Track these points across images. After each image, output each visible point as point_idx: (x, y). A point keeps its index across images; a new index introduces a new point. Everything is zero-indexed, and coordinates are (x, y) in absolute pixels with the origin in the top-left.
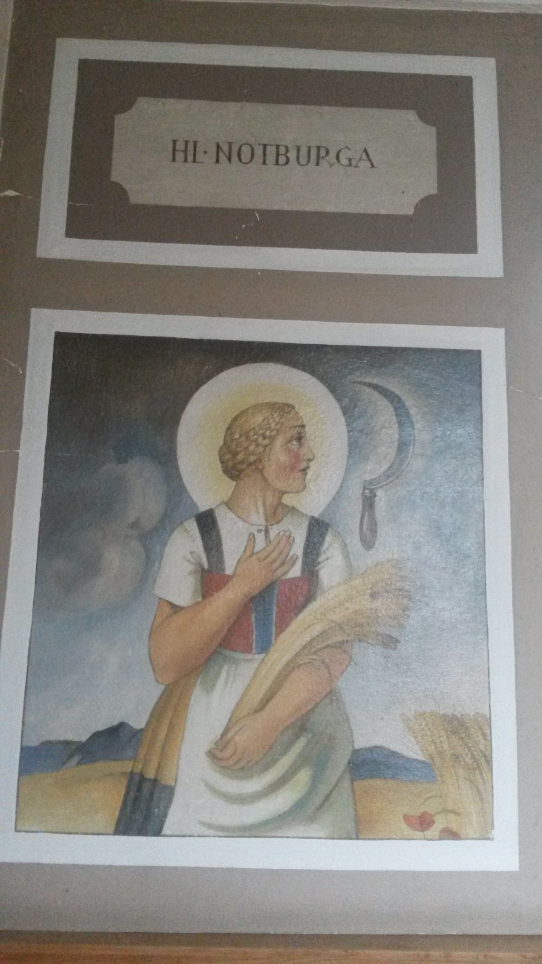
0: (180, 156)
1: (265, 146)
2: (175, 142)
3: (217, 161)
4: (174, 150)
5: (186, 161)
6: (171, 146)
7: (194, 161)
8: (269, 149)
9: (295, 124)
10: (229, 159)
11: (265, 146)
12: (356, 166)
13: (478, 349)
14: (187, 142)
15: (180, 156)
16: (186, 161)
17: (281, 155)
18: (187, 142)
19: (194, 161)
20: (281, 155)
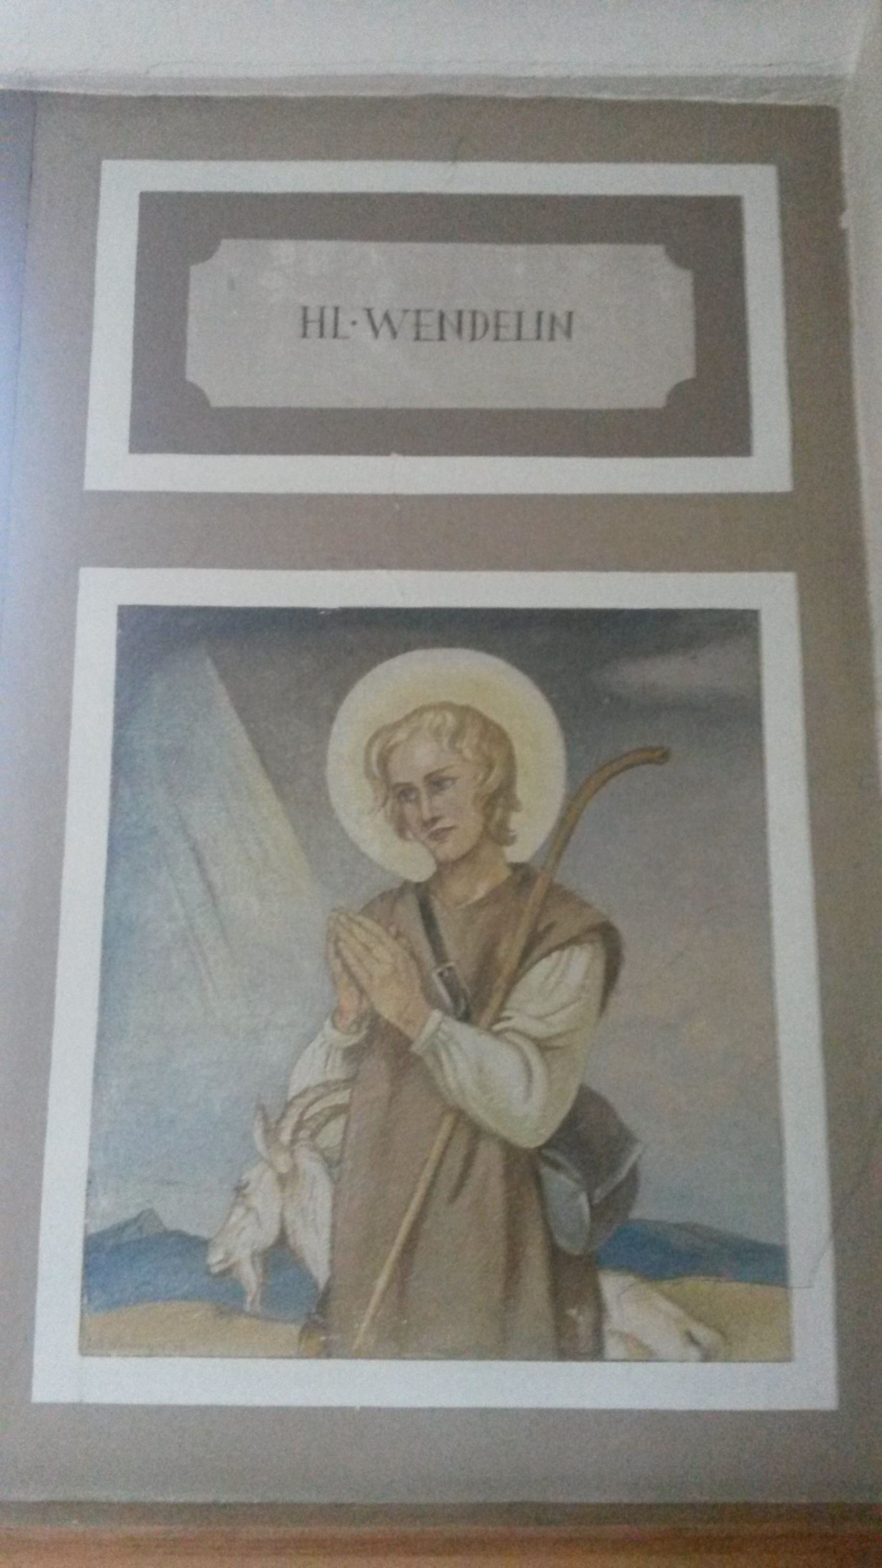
0: (313, 328)
1: (519, 337)
2: (305, 309)
3: (570, 315)
4: (305, 321)
5: (322, 335)
6: (300, 315)
7: (335, 336)
8: (512, 332)
9: (376, 373)
10: (553, 318)
11: (519, 337)
12: (406, 311)
13: (708, 1365)
14: (460, 313)
15: (313, 328)
16: (322, 335)
17: (312, 321)
18: (460, 313)
19: (335, 336)
20: (312, 321)
